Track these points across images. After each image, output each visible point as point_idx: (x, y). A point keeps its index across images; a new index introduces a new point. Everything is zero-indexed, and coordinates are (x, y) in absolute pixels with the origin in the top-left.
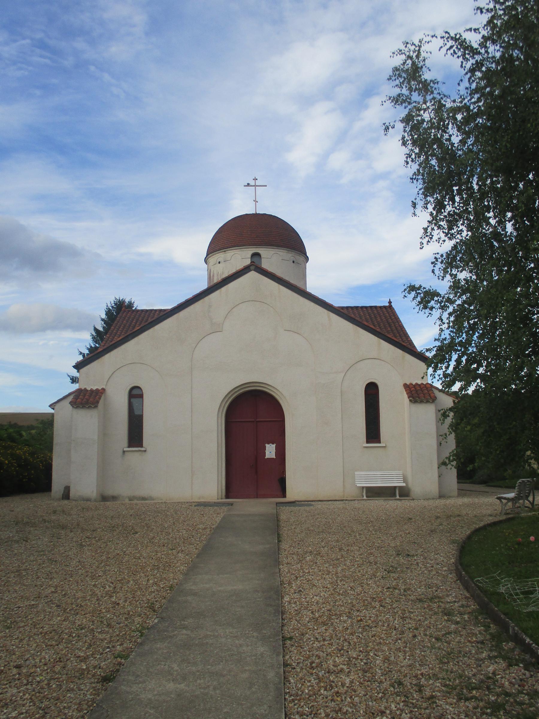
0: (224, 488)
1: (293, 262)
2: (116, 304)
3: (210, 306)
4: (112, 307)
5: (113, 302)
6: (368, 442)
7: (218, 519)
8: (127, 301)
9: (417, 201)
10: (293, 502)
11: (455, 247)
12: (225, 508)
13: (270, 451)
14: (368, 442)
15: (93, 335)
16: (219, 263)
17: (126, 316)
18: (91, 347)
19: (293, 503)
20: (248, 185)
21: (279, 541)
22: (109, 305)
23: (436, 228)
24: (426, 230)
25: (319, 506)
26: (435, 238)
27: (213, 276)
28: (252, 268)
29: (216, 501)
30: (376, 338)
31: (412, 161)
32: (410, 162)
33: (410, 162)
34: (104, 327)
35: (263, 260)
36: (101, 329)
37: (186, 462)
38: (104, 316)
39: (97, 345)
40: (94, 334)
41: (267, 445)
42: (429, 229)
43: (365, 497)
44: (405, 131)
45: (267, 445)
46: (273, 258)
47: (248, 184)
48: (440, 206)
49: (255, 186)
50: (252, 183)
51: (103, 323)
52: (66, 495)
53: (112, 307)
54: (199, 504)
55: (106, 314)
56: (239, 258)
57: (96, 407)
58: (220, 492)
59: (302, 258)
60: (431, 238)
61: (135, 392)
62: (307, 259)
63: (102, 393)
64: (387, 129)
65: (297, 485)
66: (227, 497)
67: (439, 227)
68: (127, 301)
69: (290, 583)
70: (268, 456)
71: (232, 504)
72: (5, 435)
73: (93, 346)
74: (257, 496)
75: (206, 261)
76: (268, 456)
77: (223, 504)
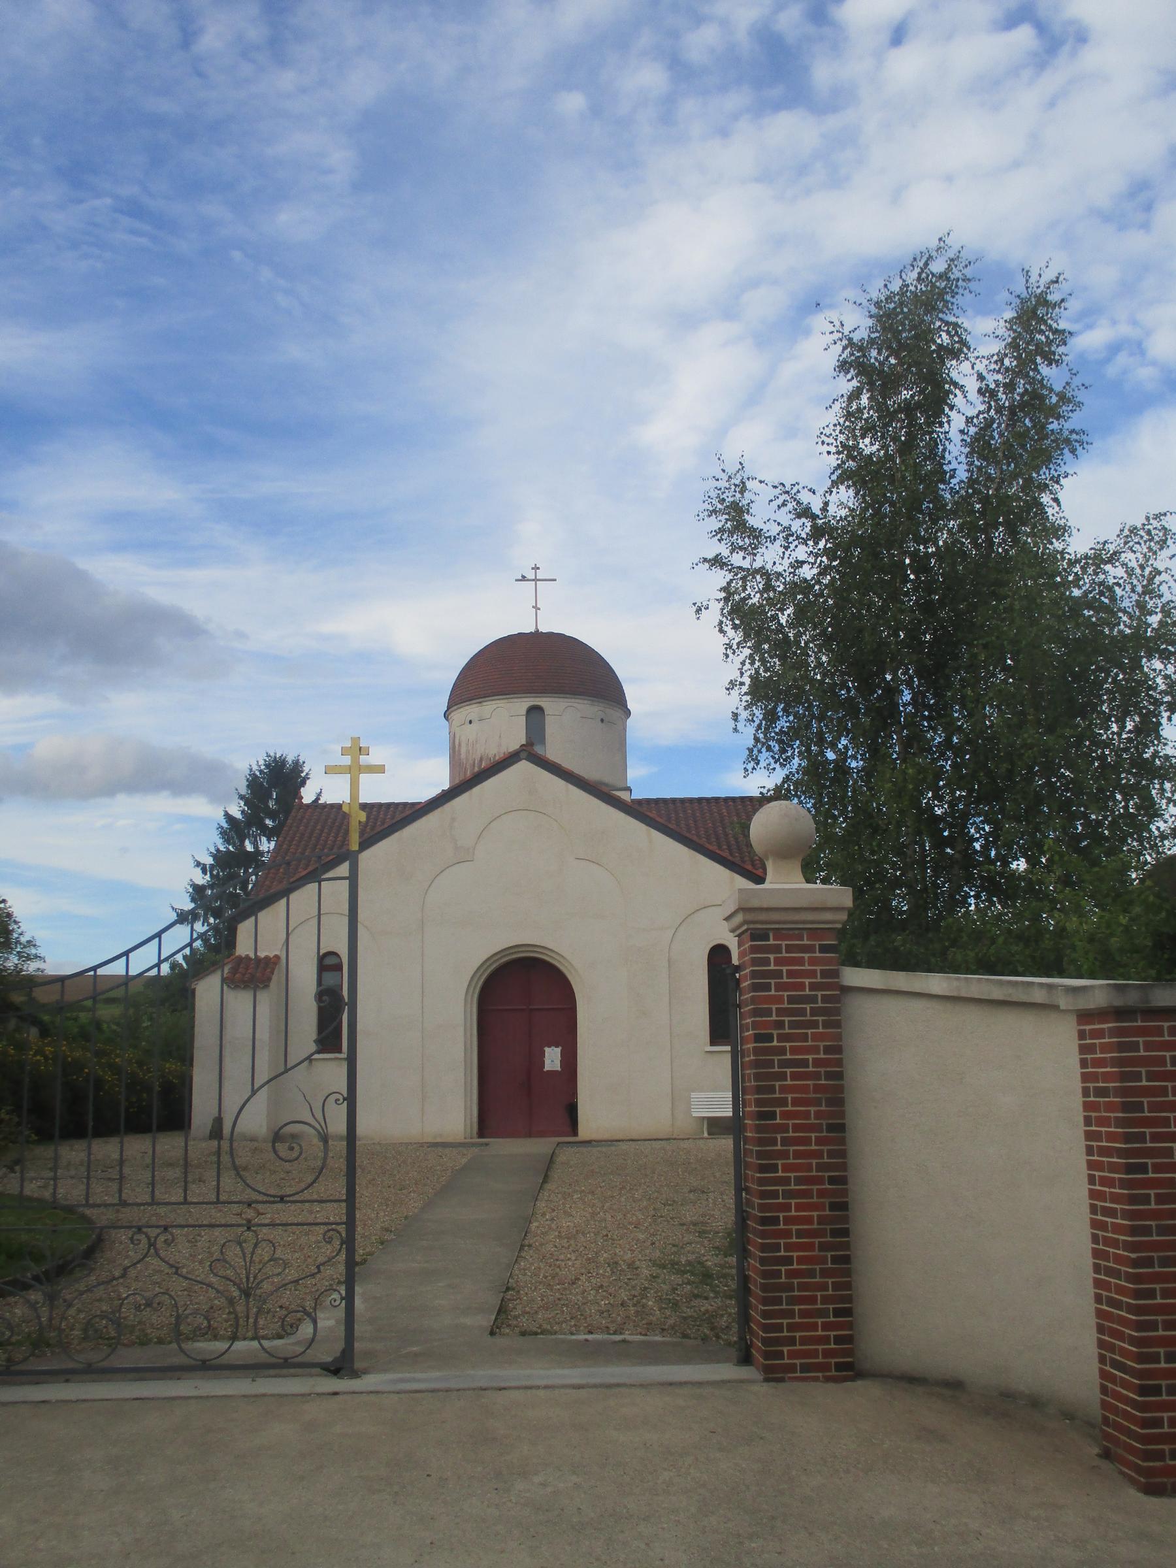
0: (475, 1119)
1: (602, 720)
2: (267, 766)
3: (453, 819)
4: (261, 771)
5: (262, 762)
6: (712, 1043)
7: (464, 1161)
8: (290, 759)
9: (739, 711)
10: (589, 1142)
11: (787, 779)
12: (476, 1150)
13: (552, 1058)
14: (712, 1043)
15: (222, 827)
16: (470, 722)
17: (303, 817)
18: (218, 850)
19: (588, 1143)
20: (524, 578)
21: (545, 1181)
22: (255, 767)
23: (764, 750)
24: (751, 750)
25: (624, 1146)
26: (763, 764)
27: (460, 745)
28: (523, 755)
29: (463, 1141)
30: (728, 871)
31: (734, 653)
32: (731, 655)
33: (731, 655)
34: (243, 812)
35: (548, 719)
36: (238, 815)
37: (418, 1075)
38: (244, 791)
39: (231, 848)
40: (225, 825)
41: (547, 1049)
42: (755, 751)
43: (706, 1135)
44: (722, 614)
45: (547, 1049)
46: (566, 719)
47: (523, 577)
48: (771, 717)
49: (536, 580)
50: (531, 575)
51: (242, 803)
52: (216, 1132)
53: (261, 771)
54: (435, 1145)
55: (248, 786)
56: (501, 723)
57: (267, 986)
58: (468, 1122)
59: (614, 713)
60: (758, 764)
61: (329, 961)
62: (628, 713)
63: (275, 964)
64: (699, 610)
65: (597, 1114)
66: (482, 1133)
67: (769, 749)
68: (290, 759)
69: (544, 1215)
70: (548, 1066)
71: (487, 1144)
72: (76, 1030)
73: (222, 848)
74: (530, 1134)
75: (446, 716)
76: (548, 1066)
77: (473, 1145)
